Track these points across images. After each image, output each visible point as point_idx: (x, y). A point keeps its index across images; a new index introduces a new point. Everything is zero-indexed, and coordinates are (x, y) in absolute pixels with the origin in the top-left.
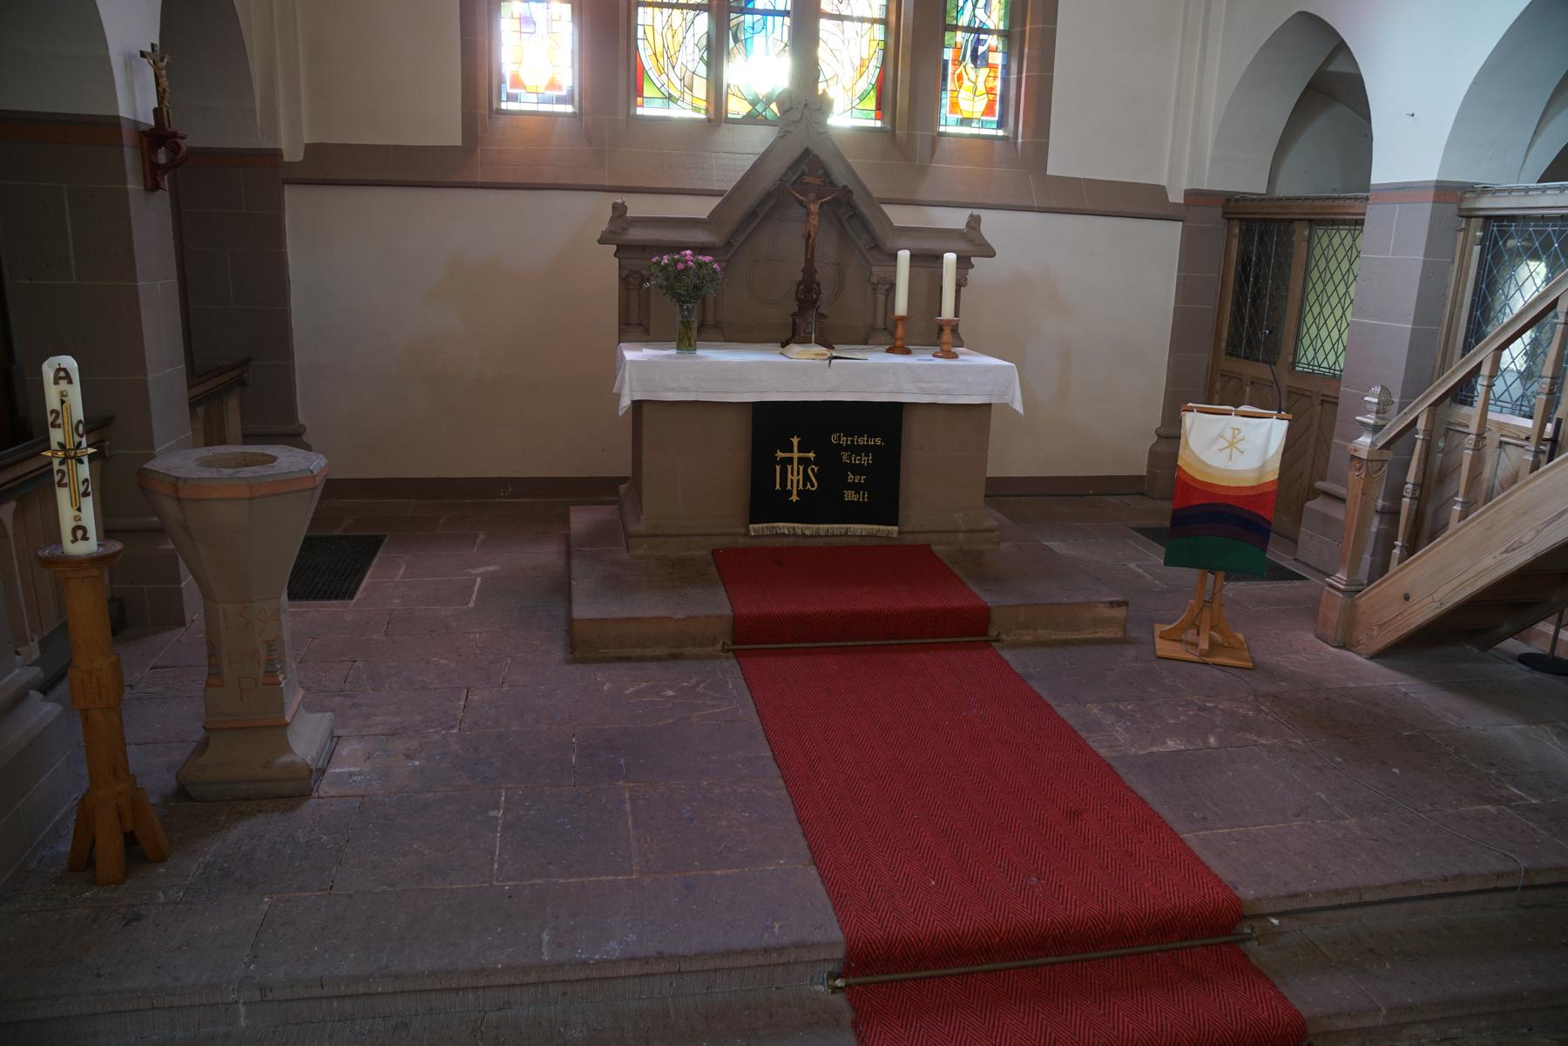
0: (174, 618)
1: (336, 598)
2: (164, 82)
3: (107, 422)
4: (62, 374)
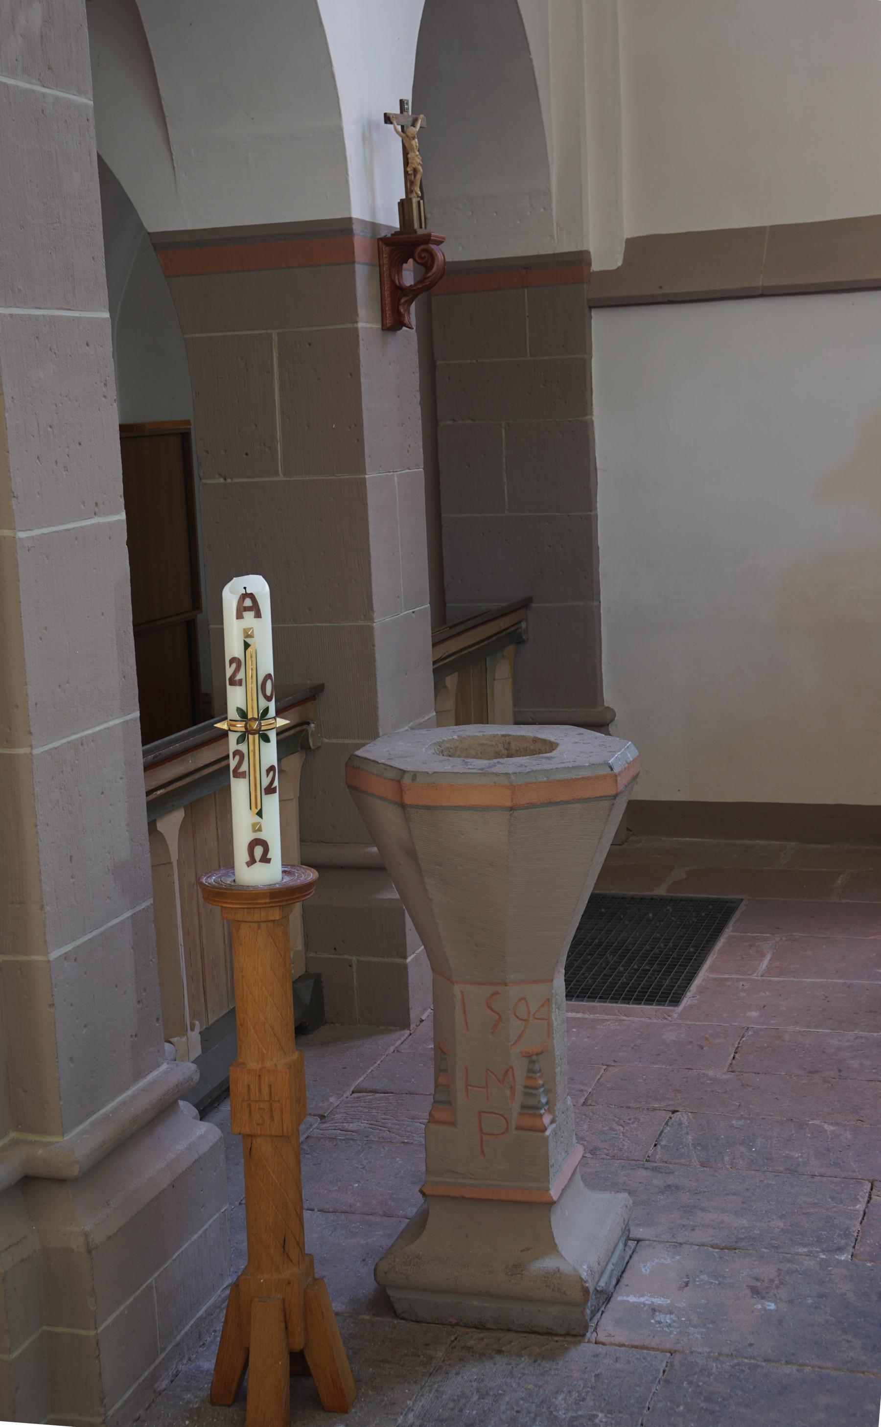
0: (397, 1017)
1: (650, 1001)
2: (416, 158)
3: (314, 694)
4: (248, 602)
